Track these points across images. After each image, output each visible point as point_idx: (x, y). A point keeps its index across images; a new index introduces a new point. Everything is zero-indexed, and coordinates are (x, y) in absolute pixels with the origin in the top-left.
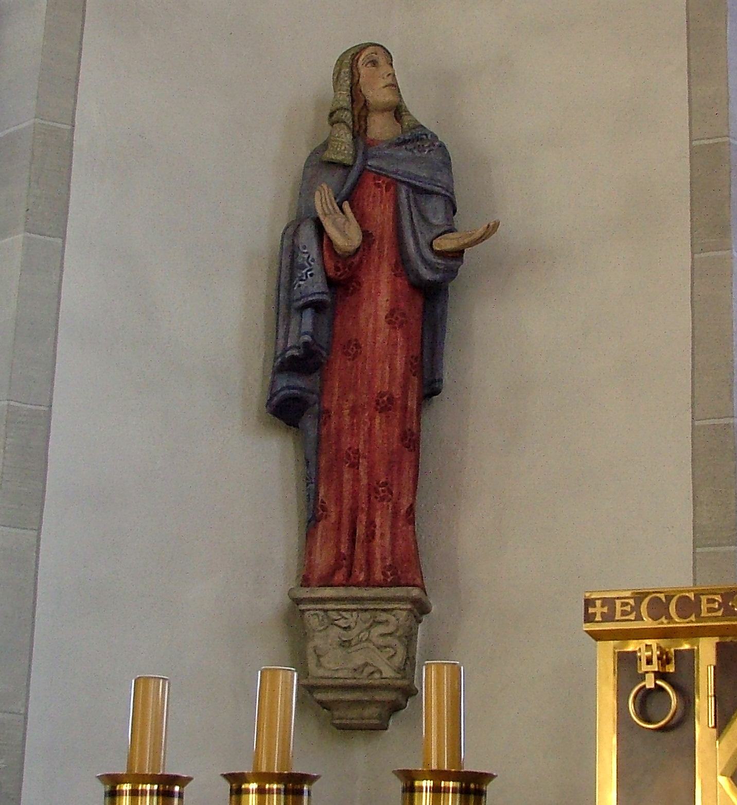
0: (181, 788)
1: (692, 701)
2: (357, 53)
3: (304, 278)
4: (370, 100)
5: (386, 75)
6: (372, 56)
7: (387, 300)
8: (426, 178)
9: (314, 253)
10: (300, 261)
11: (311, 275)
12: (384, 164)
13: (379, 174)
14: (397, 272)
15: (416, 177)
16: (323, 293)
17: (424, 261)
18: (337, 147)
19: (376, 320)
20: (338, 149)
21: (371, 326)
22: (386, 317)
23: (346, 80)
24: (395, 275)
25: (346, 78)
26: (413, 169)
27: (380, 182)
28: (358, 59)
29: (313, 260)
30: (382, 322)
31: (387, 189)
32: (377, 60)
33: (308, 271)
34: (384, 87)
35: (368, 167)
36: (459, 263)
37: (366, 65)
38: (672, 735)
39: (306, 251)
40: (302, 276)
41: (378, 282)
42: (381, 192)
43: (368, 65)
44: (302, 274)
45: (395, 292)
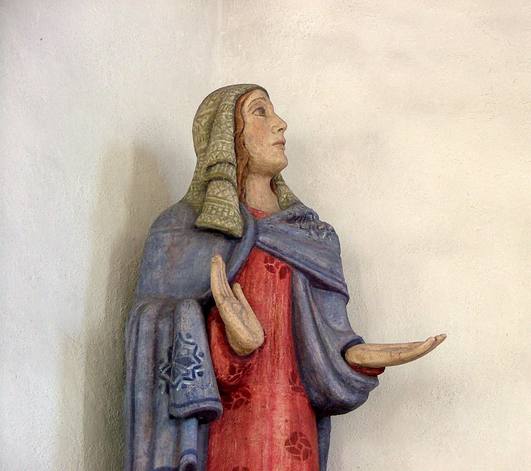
3: (191, 376)
4: (256, 159)
6: (260, 102)
7: (286, 421)
8: (325, 269)
9: (203, 347)
10: (184, 353)
11: (200, 374)
12: (278, 243)
13: (273, 255)
14: (295, 385)
15: (318, 267)
16: (216, 400)
17: (338, 375)
19: (272, 446)
20: (225, 214)
21: (266, 451)
22: (287, 443)
24: (294, 389)
25: (229, 125)
26: (311, 254)
27: (273, 265)
28: (244, 102)
29: (202, 355)
30: (281, 449)
31: (282, 276)
32: (265, 108)
33: (196, 368)
35: (259, 244)
36: (372, 382)
39: (191, 341)
40: (188, 374)
41: (273, 396)
42: (274, 277)
44: (188, 370)
45: (294, 410)
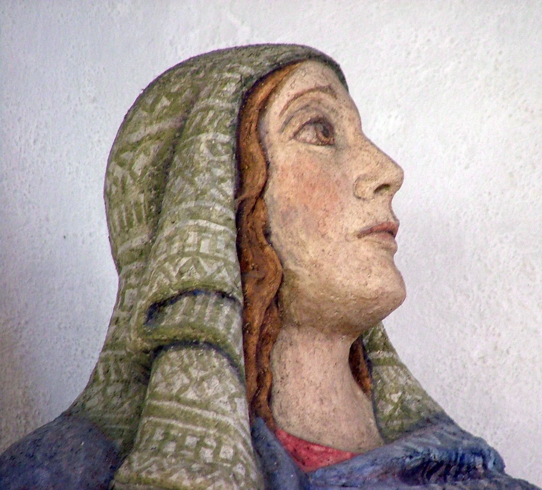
0: (186, 72)
1: (122, 126)
2: (262, 79)
5: (375, 184)
18: (201, 444)
20: (207, 454)
23: (222, 180)
25: (219, 172)
28: (266, 101)
32: (333, 119)
34: (361, 235)
37: (296, 135)
38: (198, 276)
43: (304, 135)
